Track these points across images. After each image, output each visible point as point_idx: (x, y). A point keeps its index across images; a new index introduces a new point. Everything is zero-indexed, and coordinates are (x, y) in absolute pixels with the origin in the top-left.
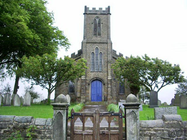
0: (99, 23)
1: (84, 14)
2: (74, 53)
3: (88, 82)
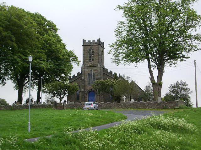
0: (93, 52)
1: (83, 46)
2: (79, 72)
3: (86, 92)
